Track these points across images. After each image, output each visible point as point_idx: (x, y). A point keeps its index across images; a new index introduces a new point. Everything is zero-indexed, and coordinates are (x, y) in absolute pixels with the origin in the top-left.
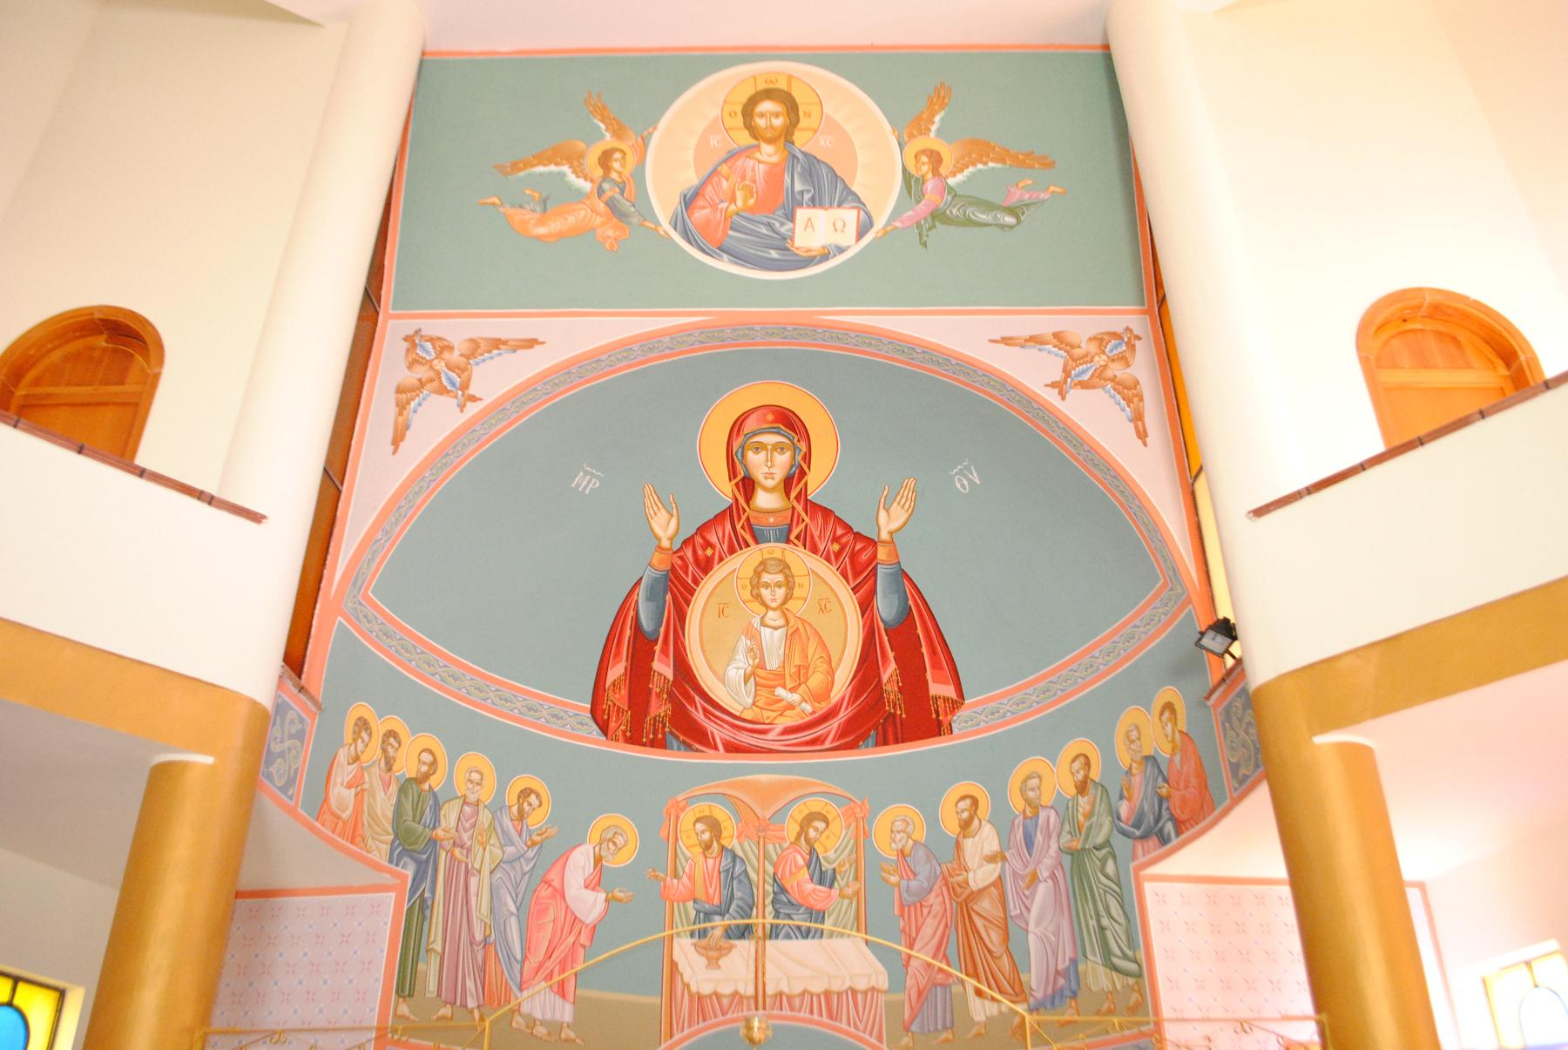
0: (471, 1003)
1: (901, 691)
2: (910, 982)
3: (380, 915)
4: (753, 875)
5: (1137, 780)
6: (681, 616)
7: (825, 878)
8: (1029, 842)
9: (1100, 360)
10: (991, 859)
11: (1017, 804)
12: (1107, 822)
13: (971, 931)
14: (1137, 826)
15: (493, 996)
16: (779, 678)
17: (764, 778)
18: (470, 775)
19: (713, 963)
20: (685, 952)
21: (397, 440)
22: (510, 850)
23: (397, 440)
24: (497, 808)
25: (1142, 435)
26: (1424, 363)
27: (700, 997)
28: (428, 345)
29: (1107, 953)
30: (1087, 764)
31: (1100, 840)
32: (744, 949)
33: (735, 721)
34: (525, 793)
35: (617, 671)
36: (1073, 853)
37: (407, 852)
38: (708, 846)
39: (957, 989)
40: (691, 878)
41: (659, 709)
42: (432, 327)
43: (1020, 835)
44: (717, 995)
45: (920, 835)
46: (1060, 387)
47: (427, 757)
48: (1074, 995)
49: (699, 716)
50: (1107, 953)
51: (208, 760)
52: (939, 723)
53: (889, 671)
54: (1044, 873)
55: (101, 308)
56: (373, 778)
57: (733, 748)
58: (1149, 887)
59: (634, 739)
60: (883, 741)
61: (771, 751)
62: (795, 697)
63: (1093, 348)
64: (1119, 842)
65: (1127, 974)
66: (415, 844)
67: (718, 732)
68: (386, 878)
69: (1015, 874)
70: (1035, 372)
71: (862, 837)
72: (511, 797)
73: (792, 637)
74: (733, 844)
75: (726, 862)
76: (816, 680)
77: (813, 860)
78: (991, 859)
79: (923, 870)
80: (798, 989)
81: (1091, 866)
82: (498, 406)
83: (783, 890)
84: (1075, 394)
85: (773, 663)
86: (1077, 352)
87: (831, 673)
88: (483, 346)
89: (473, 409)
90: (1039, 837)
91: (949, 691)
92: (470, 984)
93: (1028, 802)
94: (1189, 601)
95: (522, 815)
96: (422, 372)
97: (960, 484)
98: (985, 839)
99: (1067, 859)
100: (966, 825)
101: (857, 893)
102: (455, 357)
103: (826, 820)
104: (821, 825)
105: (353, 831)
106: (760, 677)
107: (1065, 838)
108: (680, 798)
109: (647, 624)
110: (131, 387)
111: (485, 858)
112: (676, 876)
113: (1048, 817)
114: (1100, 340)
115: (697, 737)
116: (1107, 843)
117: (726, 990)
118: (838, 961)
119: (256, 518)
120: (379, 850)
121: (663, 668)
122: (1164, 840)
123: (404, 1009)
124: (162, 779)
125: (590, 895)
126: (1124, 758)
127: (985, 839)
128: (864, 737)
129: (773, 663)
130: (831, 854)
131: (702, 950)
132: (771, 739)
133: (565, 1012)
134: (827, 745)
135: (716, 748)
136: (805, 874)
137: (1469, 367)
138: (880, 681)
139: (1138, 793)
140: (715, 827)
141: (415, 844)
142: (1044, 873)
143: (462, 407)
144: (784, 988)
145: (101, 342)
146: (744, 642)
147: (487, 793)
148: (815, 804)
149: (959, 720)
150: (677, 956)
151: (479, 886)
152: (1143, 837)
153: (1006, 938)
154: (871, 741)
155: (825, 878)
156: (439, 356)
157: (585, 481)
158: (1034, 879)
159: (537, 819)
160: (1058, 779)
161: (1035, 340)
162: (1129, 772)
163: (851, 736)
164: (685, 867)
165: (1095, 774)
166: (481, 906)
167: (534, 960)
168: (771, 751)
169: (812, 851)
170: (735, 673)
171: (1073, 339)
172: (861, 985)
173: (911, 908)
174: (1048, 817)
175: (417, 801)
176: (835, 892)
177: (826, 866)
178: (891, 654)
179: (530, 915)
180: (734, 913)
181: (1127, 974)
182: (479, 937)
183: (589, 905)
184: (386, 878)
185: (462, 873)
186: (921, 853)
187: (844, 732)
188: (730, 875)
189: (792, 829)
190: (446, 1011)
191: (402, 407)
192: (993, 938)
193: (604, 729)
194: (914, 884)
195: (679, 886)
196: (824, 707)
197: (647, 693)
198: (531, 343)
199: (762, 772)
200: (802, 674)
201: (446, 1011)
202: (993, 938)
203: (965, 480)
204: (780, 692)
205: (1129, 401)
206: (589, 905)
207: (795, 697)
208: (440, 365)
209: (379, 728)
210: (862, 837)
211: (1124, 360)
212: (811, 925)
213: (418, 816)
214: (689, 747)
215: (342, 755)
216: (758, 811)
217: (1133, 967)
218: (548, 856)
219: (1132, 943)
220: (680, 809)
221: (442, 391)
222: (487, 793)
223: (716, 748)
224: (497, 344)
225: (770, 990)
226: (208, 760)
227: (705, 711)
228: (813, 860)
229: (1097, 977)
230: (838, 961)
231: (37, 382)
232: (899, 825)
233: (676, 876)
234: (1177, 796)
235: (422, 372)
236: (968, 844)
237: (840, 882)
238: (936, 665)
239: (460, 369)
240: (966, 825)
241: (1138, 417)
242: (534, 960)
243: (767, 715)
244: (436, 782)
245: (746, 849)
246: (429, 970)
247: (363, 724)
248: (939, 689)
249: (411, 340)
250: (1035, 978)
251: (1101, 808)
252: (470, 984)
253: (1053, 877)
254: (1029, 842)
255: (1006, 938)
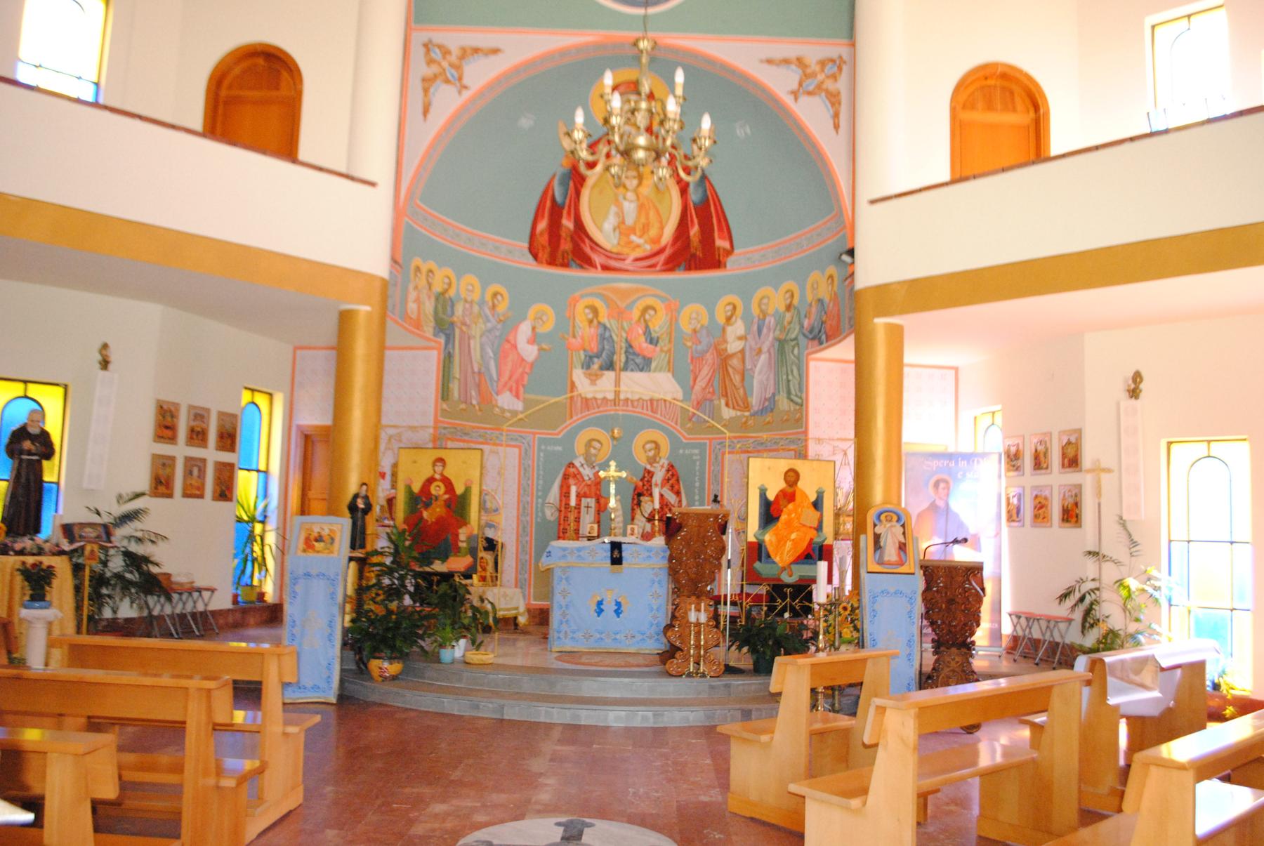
0: (474, 402)
1: (698, 243)
2: (693, 397)
3: (430, 361)
4: (615, 338)
5: (814, 310)
6: (578, 193)
7: (653, 341)
8: (760, 331)
9: (821, 77)
10: (740, 338)
11: (755, 311)
12: (797, 328)
13: (725, 375)
14: (811, 331)
15: (486, 399)
16: (632, 230)
17: (623, 285)
18: (468, 287)
19: (593, 382)
20: (579, 375)
21: (426, 111)
22: (489, 325)
23: (426, 111)
24: (482, 303)
25: (836, 127)
26: (990, 107)
27: (587, 400)
28: (437, 50)
29: (789, 393)
30: (792, 296)
31: (793, 336)
32: (609, 376)
33: (608, 254)
34: (495, 295)
35: (543, 225)
36: (779, 340)
37: (441, 330)
38: (591, 322)
39: (716, 402)
40: (582, 338)
41: (566, 246)
42: (439, 37)
43: (755, 327)
44: (596, 399)
45: (705, 321)
46: (795, 94)
47: (447, 281)
48: (772, 410)
49: (587, 250)
50: (789, 393)
51: (368, 308)
52: (719, 262)
53: (694, 231)
54: (765, 349)
55: (261, 45)
56: (424, 296)
57: (606, 268)
58: (812, 364)
59: (552, 262)
60: (689, 268)
61: (626, 271)
62: (640, 241)
63: (818, 68)
64: (801, 337)
65: (797, 404)
66: (444, 326)
67: (598, 259)
68: (433, 344)
69: (751, 348)
70: (780, 83)
71: (674, 321)
72: (488, 297)
73: (641, 207)
74: (604, 320)
75: (601, 330)
76: (653, 232)
77: (647, 331)
78: (740, 338)
79: (705, 341)
80: (636, 397)
81: (787, 348)
82: (481, 93)
83: (631, 346)
84: (804, 99)
85: (630, 221)
86: (809, 71)
87: (662, 228)
88: (469, 51)
89: (466, 94)
90: (765, 331)
91: (726, 245)
92: (473, 393)
93: (762, 311)
94: (845, 227)
95: (494, 306)
96: (434, 69)
97: (740, 132)
98: (738, 328)
99: (777, 344)
100: (729, 319)
101: (669, 351)
102: (453, 58)
103: (654, 309)
104: (652, 312)
105: (418, 325)
106: (623, 230)
107: (777, 333)
108: (577, 294)
109: (559, 198)
110: (284, 92)
111: (476, 330)
112: (574, 337)
113: (771, 321)
114: (823, 63)
115: (585, 261)
116: (796, 339)
117: (599, 396)
118: (657, 384)
119: (372, 184)
120: (429, 330)
121: (568, 223)
122: (821, 343)
123: (445, 406)
124: (345, 319)
125: (529, 347)
126: (809, 298)
127: (738, 328)
128: (678, 265)
129: (630, 221)
130: (657, 329)
131: (589, 376)
132: (628, 264)
133: (519, 406)
134: (658, 268)
135: (595, 267)
136: (642, 339)
137: (1014, 110)
138: (688, 237)
139: (813, 316)
140: (595, 311)
141: (444, 326)
142: (765, 349)
143: (460, 92)
144: (629, 396)
145: (261, 61)
146: (613, 209)
147: (476, 296)
148: (650, 301)
149: (731, 262)
150: (575, 378)
151: (475, 345)
152: (813, 339)
153: (743, 380)
154: (682, 267)
155: (653, 341)
156: (444, 58)
157: (525, 122)
158: (759, 352)
159: (502, 307)
160: (777, 302)
161: (786, 62)
162: (811, 305)
163: (672, 264)
164: (579, 333)
165: (796, 302)
166: (476, 354)
167: (503, 380)
168: (626, 271)
169: (647, 326)
170: (609, 224)
171: (807, 61)
172: (668, 398)
173: (697, 360)
174: (771, 321)
175: (444, 302)
176: (658, 349)
177: (654, 335)
178: (696, 220)
179: (501, 357)
180: (604, 359)
181: (797, 404)
182: (476, 370)
183: (529, 352)
184: (433, 344)
185: (466, 338)
186: (704, 332)
187: (667, 262)
188: (603, 338)
189: (636, 314)
190: (463, 406)
191: (426, 91)
192: (737, 379)
193: (535, 257)
194: (699, 348)
195: (575, 342)
196: (656, 247)
197: (560, 238)
198: (495, 51)
199: (622, 282)
200: (645, 228)
201: (463, 406)
202: (737, 379)
203: (742, 131)
204: (633, 238)
205: (833, 105)
206: (529, 352)
207: (640, 241)
208: (445, 64)
209: (424, 269)
210: (674, 321)
211: (834, 77)
212: (645, 365)
213: (444, 307)
214: (582, 267)
215: (411, 287)
216: (619, 303)
217: (799, 401)
218: (509, 324)
219: (800, 389)
220: (576, 301)
221: (447, 81)
222: (476, 296)
223: (595, 267)
224: (476, 51)
225: (622, 397)
226: (368, 308)
227: (592, 248)
228: (647, 331)
229: (783, 403)
230: (657, 384)
231: (230, 87)
232: (694, 315)
233: (574, 337)
234: (829, 323)
235: (434, 69)
236: (729, 329)
237: (661, 343)
238: (720, 229)
239: (458, 68)
240: (729, 319)
241: (836, 116)
242: (503, 380)
243: (626, 250)
244: (452, 293)
245: (612, 324)
246: (455, 387)
247: (418, 269)
248: (721, 243)
249: (427, 46)
250: (754, 401)
251: (796, 319)
252: (473, 393)
253: (769, 351)
254: (760, 331)
255: (743, 380)
